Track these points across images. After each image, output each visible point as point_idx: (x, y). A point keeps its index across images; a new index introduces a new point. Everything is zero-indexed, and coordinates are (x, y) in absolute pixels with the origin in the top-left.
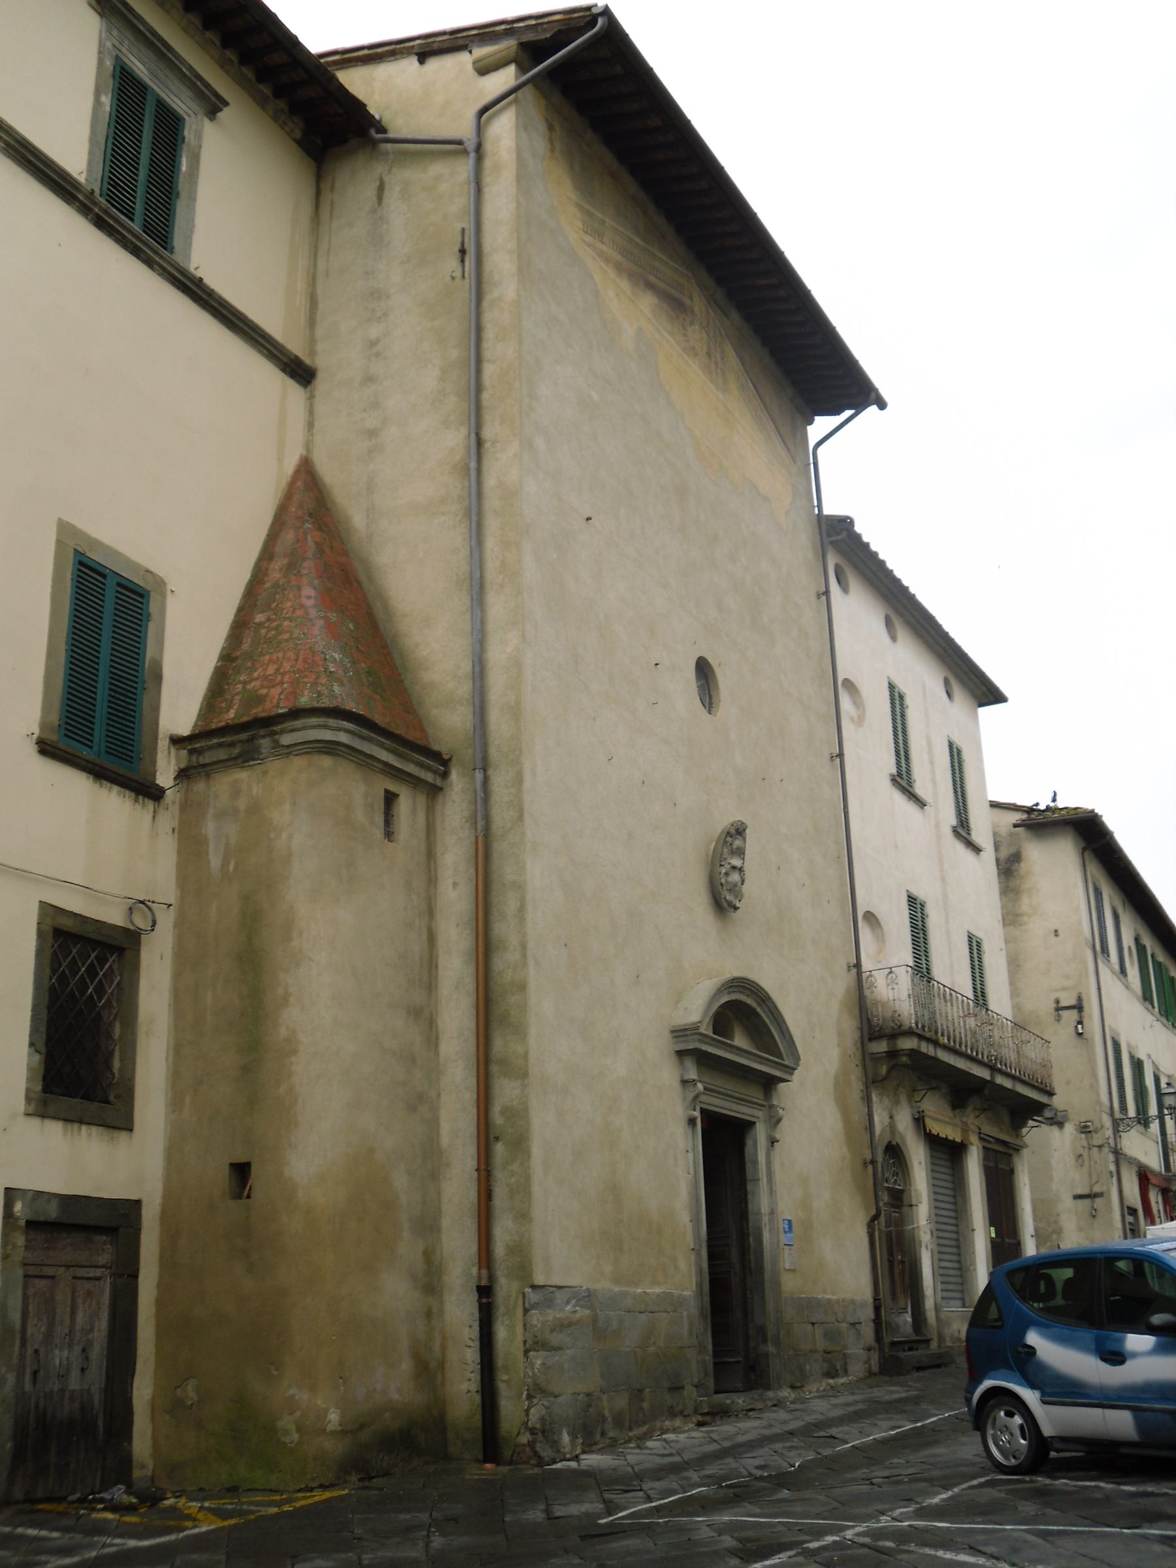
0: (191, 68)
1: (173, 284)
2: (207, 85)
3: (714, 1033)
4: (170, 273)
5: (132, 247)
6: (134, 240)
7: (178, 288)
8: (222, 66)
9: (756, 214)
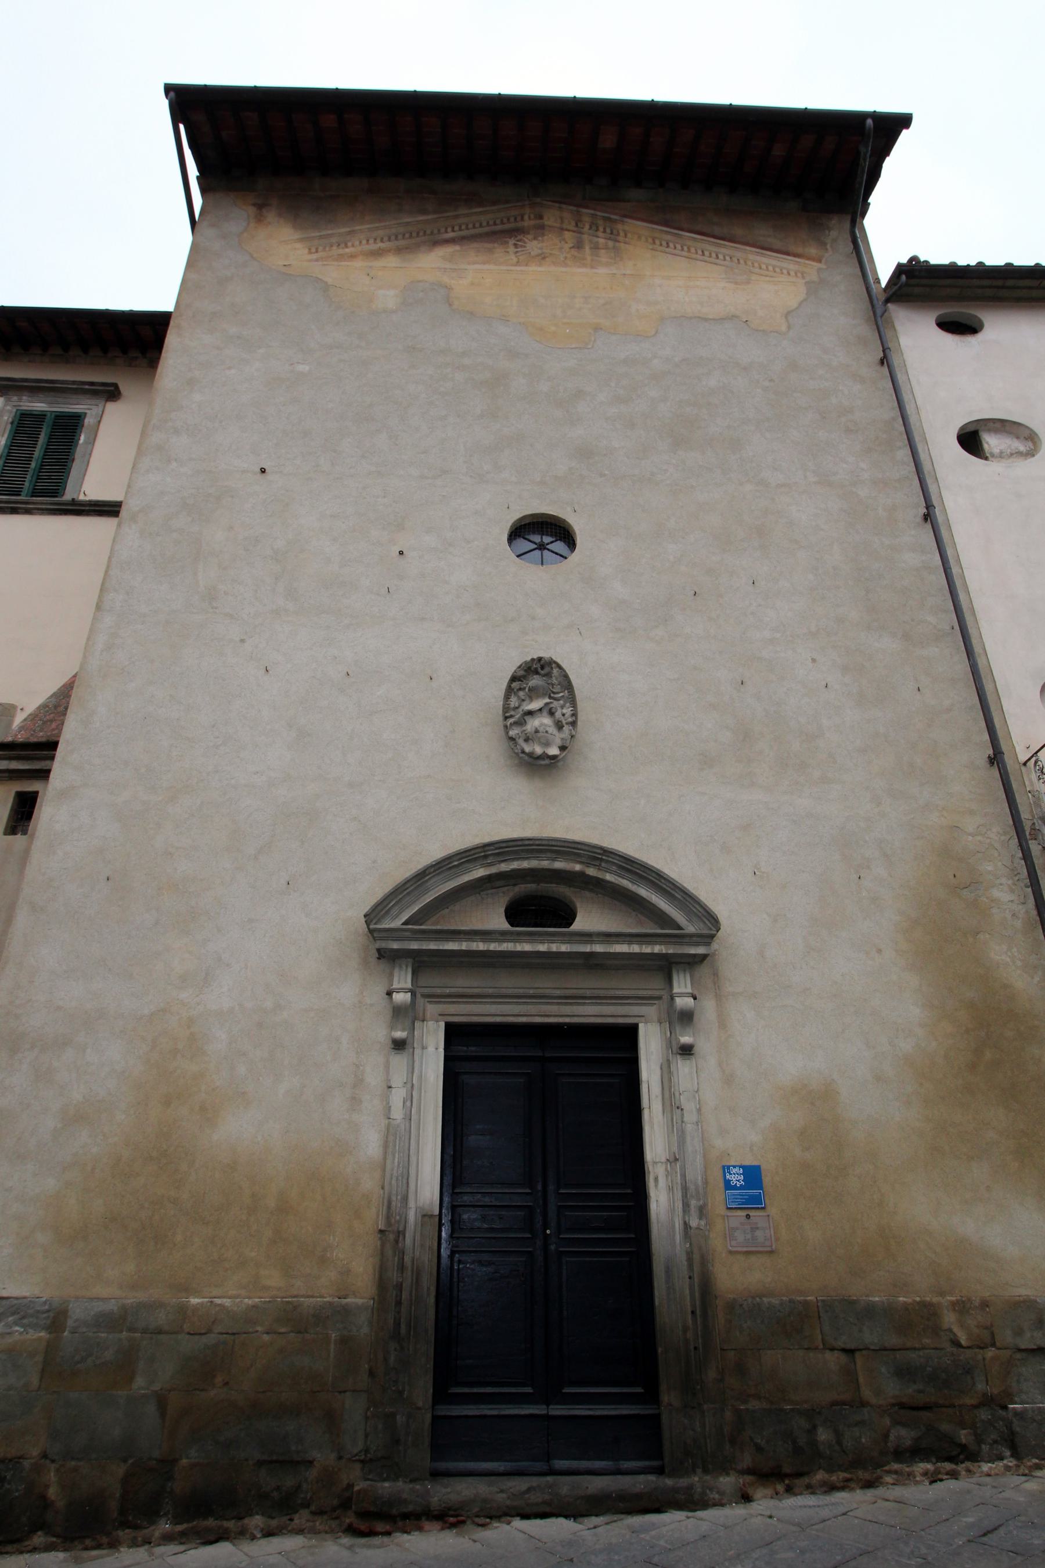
0: (74, 382)
1: (55, 514)
2: (92, 384)
3: (512, 925)
4: (47, 509)
5: (10, 510)
6: (6, 505)
7: (61, 514)
8: (130, 366)
9: (415, 91)
